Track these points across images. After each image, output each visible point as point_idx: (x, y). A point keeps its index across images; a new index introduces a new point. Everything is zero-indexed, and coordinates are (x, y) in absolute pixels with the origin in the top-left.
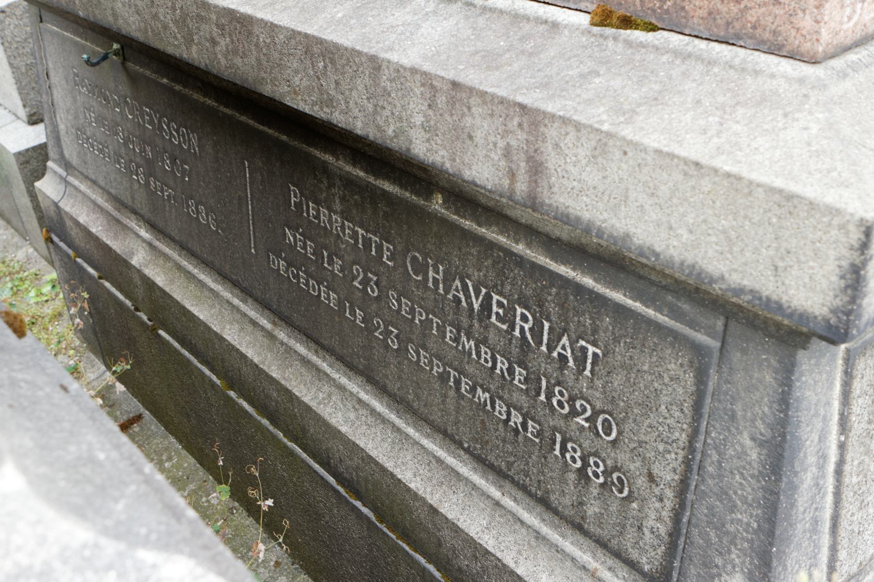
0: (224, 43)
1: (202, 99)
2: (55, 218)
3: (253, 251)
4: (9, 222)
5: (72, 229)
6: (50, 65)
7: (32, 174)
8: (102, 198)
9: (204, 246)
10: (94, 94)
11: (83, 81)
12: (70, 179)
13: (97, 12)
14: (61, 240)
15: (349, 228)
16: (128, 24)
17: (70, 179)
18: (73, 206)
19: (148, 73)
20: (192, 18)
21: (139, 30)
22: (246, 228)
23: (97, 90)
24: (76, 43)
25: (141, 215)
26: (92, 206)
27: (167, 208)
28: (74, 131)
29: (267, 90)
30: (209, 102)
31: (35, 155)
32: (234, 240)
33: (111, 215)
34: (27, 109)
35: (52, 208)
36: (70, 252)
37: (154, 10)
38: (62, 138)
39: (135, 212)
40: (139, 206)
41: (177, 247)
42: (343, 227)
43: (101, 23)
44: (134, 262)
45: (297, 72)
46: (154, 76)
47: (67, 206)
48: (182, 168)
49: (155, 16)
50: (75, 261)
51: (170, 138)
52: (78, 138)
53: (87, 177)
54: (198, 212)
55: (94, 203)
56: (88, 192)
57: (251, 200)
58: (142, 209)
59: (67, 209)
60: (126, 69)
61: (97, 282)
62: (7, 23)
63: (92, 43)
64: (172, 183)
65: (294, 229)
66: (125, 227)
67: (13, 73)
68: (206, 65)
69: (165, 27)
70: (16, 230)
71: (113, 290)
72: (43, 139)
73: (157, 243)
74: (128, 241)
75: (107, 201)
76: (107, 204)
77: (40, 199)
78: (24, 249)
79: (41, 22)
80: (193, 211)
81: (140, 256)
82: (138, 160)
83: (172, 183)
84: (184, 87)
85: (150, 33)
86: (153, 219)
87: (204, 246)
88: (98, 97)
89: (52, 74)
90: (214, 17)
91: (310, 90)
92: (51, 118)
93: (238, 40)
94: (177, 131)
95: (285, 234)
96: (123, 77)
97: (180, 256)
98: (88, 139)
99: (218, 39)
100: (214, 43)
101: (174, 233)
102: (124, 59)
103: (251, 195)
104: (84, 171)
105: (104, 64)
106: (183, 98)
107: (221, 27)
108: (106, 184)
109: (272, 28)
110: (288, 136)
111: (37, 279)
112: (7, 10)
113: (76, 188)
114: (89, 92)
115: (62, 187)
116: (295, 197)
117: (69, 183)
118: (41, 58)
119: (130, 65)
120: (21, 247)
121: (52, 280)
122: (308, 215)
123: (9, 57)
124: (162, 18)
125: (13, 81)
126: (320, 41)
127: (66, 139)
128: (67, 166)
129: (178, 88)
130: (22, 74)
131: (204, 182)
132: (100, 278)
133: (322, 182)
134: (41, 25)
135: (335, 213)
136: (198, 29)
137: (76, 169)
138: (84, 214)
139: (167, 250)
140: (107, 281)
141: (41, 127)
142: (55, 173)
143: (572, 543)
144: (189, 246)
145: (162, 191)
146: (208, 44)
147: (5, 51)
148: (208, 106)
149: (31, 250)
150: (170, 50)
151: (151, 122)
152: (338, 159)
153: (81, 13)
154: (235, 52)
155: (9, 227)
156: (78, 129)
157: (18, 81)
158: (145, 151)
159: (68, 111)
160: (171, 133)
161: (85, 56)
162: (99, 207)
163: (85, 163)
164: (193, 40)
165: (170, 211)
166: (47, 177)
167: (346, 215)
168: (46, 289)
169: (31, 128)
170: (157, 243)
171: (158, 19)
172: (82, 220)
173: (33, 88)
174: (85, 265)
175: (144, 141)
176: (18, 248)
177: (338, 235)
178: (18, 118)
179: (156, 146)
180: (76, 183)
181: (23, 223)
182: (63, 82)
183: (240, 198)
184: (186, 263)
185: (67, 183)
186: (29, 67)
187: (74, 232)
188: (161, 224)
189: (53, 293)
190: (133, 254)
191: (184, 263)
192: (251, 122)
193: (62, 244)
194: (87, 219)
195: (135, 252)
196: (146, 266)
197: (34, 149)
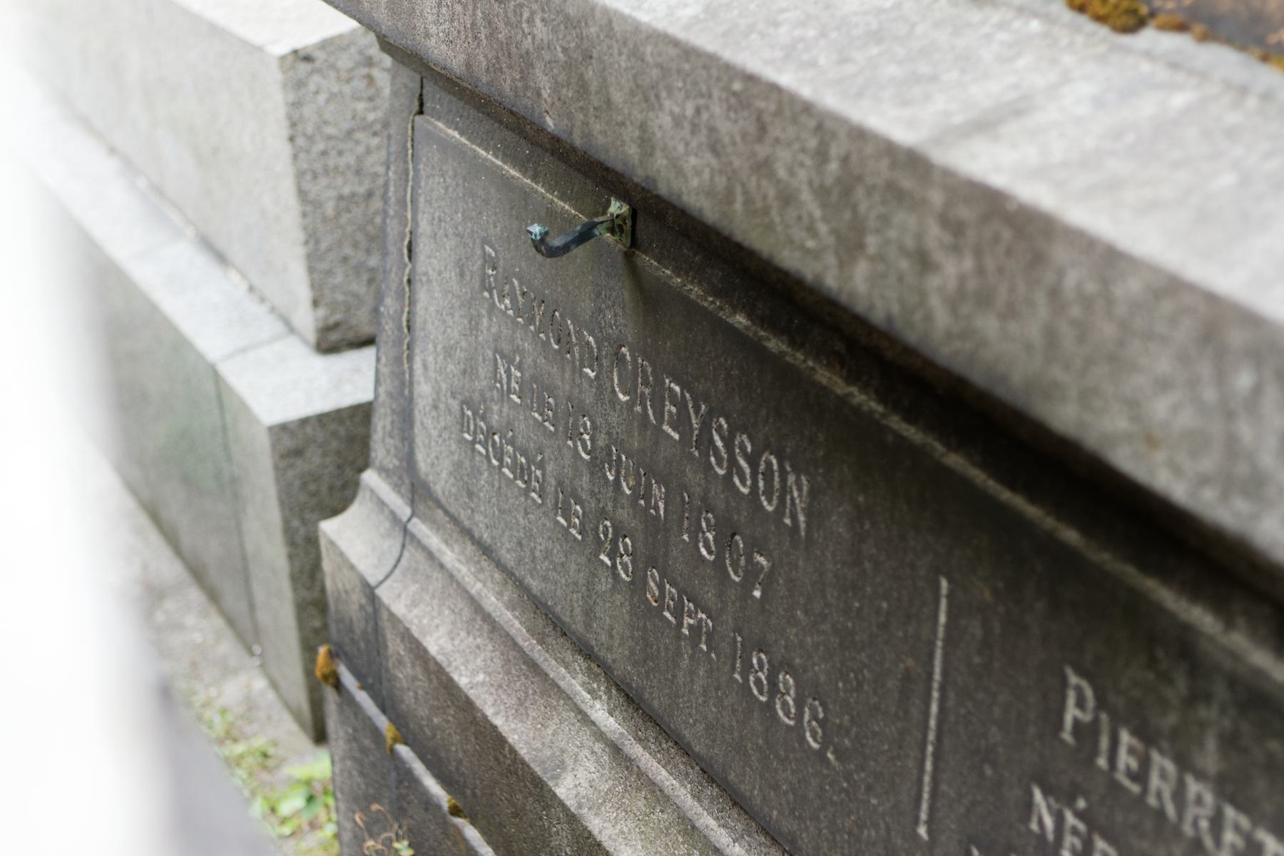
0: (952, 270)
1: (840, 387)
2: (359, 626)
3: (922, 831)
4: (213, 596)
5: (400, 662)
6: (424, 226)
7: (304, 485)
8: (499, 594)
9: (776, 787)
10: (531, 320)
11: (507, 280)
12: (420, 528)
13: (597, 127)
14: (364, 687)
15: (1237, 828)
16: (680, 172)
17: (420, 528)
18: (414, 604)
19: (695, 291)
20: (870, 191)
21: (710, 193)
22: (911, 763)
23: (543, 313)
24: (506, 182)
25: (601, 664)
26: (467, 613)
27: (685, 662)
28: (455, 405)
29: (1064, 416)
30: (859, 397)
31: (320, 436)
32: (869, 788)
33: (515, 645)
34: (322, 312)
35: (357, 598)
36: (383, 722)
37: (762, 151)
38: (418, 416)
39: (587, 653)
40: (603, 638)
41: (694, 773)
42: (1217, 823)
43: (602, 157)
44: (565, 789)
45: (1164, 385)
46: (710, 303)
47: (399, 600)
48: (750, 559)
49: (764, 167)
50: (392, 750)
51: (729, 476)
52: (463, 424)
53: (467, 533)
54: (774, 689)
55: (476, 606)
56: (464, 571)
57: (943, 689)
58: (609, 649)
59: (399, 608)
61: (445, 825)
62: (312, 87)
63: (550, 189)
64: (710, 596)
65: (1063, 795)
66: (551, 688)
67: (304, 215)
69: (787, 198)
70: (231, 621)
73: (635, 750)
74: (552, 727)
75: (511, 606)
76: (509, 615)
77: (327, 565)
78: (243, 678)
79: (421, 112)
80: (758, 682)
81: (582, 775)
82: (623, 514)
83: (710, 596)
84: (792, 343)
85: (738, 206)
86: (636, 681)
87: (776, 787)
88: (539, 331)
89: (423, 248)
90: (937, 198)
91: (1196, 442)
92: (398, 360)
93: (1000, 270)
94: (753, 460)
95: (1029, 805)
96: (622, 291)
97: (697, 797)
98: (491, 432)
99: (938, 256)
100: (924, 262)
101: (693, 734)
102: (634, 243)
103: (945, 673)
104: (463, 515)
105: (579, 252)
106: (787, 376)
107: (956, 228)
108: (520, 561)
109: (1110, 259)
110: (1085, 531)
111: (265, 768)
112: (320, 56)
113: (431, 556)
114: (518, 313)
115: (392, 546)
116: (1081, 704)
117: (413, 537)
118: (402, 203)
119: (646, 261)
120: (235, 672)
121: (308, 783)
122: (1112, 759)
123: (300, 175)
124: (782, 173)
125: (300, 236)
126: (1251, 319)
127: (429, 422)
128: (418, 492)
129: (775, 344)
130: (325, 220)
131: (806, 612)
132: (455, 811)
133: (1170, 682)
134: (418, 118)
135: (1200, 776)
136: (885, 220)
137: (439, 505)
138: (442, 630)
139: (662, 775)
140: (473, 823)
142: (381, 504)
143: (583, 684)
144: (732, 777)
145: (679, 613)
146: (904, 264)
148: (856, 410)
149: (260, 684)
150: (789, 259)
151: (681, 422)
153: (550, 122)
154: (984, 299)
155: (212, 610)
156: (467, 402)
157: (312, 238)
158: (647, 496)
159: (449, 352)
160: (733, 462)
161: (536, 229)
162: (487, 617)
163: (470, 495)
164: (861, 246)
165: (692, 673)
166: (355, 512)
167: (1231, 788)
168: (293, 803)
169: (322, 363)
170: (635, 750)
171: (771, 175)
172: (435, 644)
173: (345, 259)
174: (419, 768)
175: (650, 469)
176: (227, 671)
178: (291, 330)
179: (684, 487)
180: (434, 541)
181: (252, 607)
182: (452, 275)
183: (907, 677)
184: (712, 823)
185: (408, 536)
186: (346, 202)
187: (405, 674)
188: (657, 702)
189: (304, 819)
190: (562, 765)
191: (706, 821)
192: (978, 476)
193: (363, 698)
194: (449, 647)
195: (569, 762)
196: (596, 808)
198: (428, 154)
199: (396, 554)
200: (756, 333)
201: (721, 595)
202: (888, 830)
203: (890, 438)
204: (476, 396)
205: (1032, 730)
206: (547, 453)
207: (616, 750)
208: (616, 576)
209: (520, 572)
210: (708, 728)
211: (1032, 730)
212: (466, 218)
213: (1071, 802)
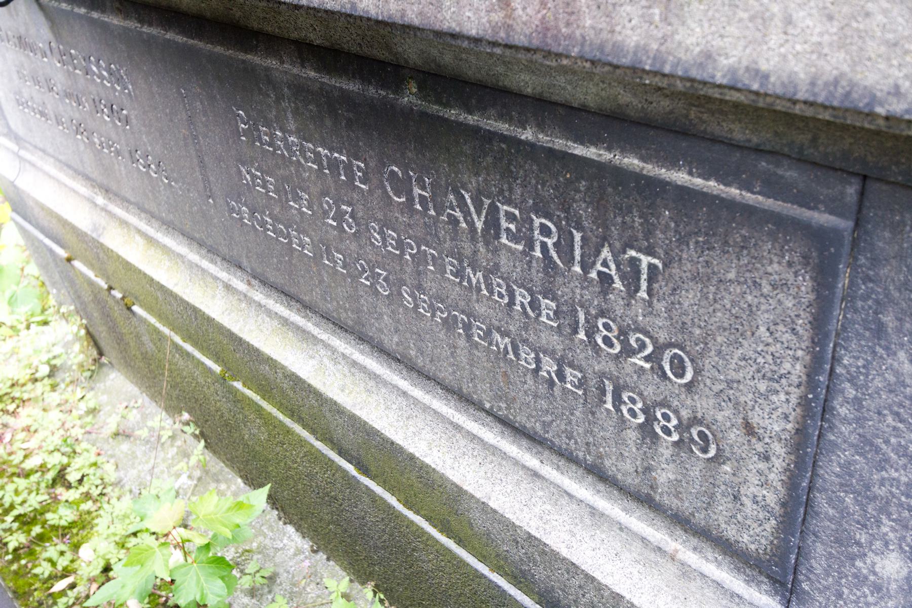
12: (22, 153)
17: (22, 153)
32: (188, 190)
101: (129, 195)
106: (285, 322)
129: (95, 15)
152: (282, 62)
156: (15, 93)
185: (22, 159)
187: (37, 211)
200: (743, 197)
203: (145, 36)
205: (231, 141)
207: (228, 287)
210: (133, 189)
211: (231, 141)
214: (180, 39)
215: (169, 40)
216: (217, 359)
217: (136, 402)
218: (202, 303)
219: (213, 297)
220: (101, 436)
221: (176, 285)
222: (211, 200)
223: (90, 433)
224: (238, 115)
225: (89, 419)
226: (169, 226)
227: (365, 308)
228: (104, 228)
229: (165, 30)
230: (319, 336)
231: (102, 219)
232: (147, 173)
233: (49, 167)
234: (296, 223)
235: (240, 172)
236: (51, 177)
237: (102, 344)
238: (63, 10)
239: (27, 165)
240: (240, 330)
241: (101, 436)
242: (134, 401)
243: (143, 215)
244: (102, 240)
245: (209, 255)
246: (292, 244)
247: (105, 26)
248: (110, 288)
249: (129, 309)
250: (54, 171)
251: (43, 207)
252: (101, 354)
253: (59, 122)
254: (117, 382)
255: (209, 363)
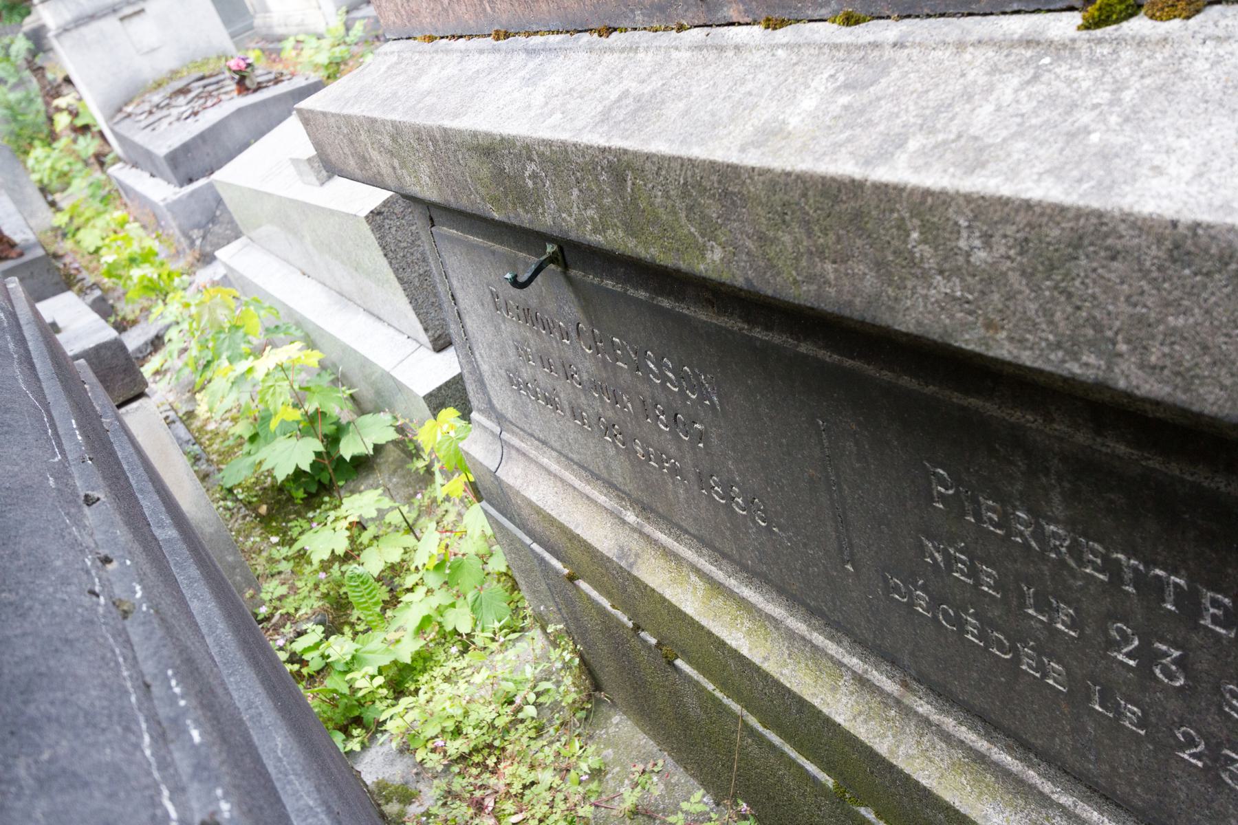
6: (455, 283)
12: (505, 436)
17: (505, 436)
28: (503, 372)
32: (805, 545)
40: (620, 479)
46: (619, 288)
60: (570, 281)
68: (747, 280)
71: (594, 594)
72: (455, 370)
73: (649, 529)
89: (460, 295)
106: (980, 758)
108: (563, 446)
123: (396, 271)
128: (500, 419)
129: (666, 303)
141: (450, 353)
147: (390, 263)
152: (1049, 419)
159: (490, 346)
163: (526, 417)
170: (649, 529)
177: (1062, 563)
180: (515, 441)
182: (478, 306)
185: (504, 444)
187: (526, 512)
197: (447, 384)
198: (444, 247)
199: (500, 452)
201: (679, 449)
202: (826, 568)
204: (512, 366)
205: (909, 504)
206: (558, 388)
207: (862, 682)
208: (617, 447)
209: (565, 451)
212: (474, 275)
213: (952, 542)
214: (825, 355)
215: (806, 356)
216: (828, 768)
217: (655, 765)
218: (814, 694)
219: (834, 689)
220: (614, 812)
221: (766, 659)
222: (849, 567)
223: (185, 350)
224: (935, 474)
225: (594, 786)
226: (754, 575)
227: (1182, 796)
228: (637, 555)
229: (798, 339)
230: (1055, 797)
231: (635, 544)
232: (728, 507)
233: (548, 460)
234: (1036, 639)
235: (922, 547)
236: (549, 473)
237: (604, 678)
238: (608, 290)
239: (513, 452)
240: (891, 752)
241: (614, 812)
242: (652, 762)
243: (705, 551)
244: (635, 573)
245: (828, 629)
246: (1019, 662)
247: (682, 320)
248: (637, 628)
249: (671, 663)
250: (554, 467)
251: (538, 511)
252: (597, 687)
253: (575, 414)
254: (620, 725)
255: (823, 777)
